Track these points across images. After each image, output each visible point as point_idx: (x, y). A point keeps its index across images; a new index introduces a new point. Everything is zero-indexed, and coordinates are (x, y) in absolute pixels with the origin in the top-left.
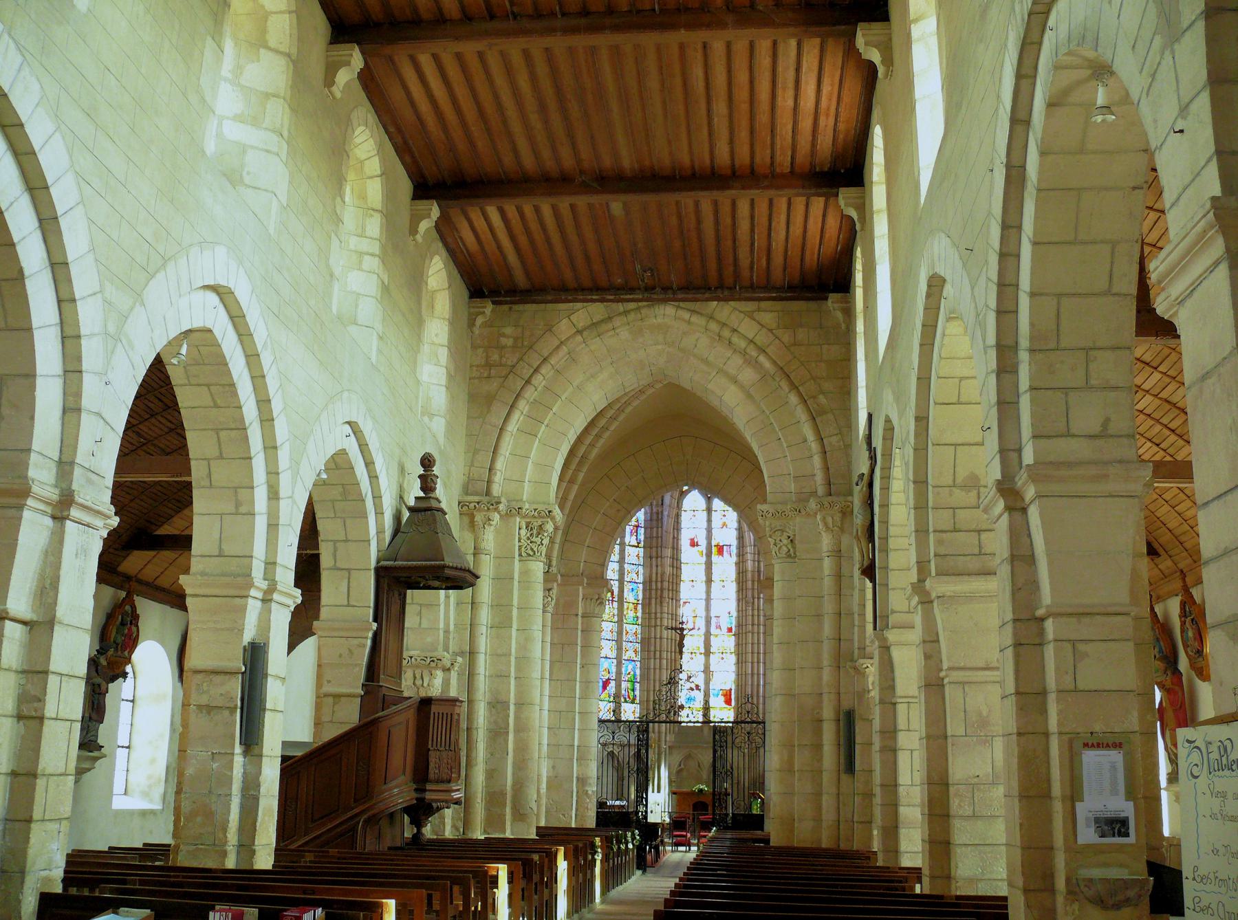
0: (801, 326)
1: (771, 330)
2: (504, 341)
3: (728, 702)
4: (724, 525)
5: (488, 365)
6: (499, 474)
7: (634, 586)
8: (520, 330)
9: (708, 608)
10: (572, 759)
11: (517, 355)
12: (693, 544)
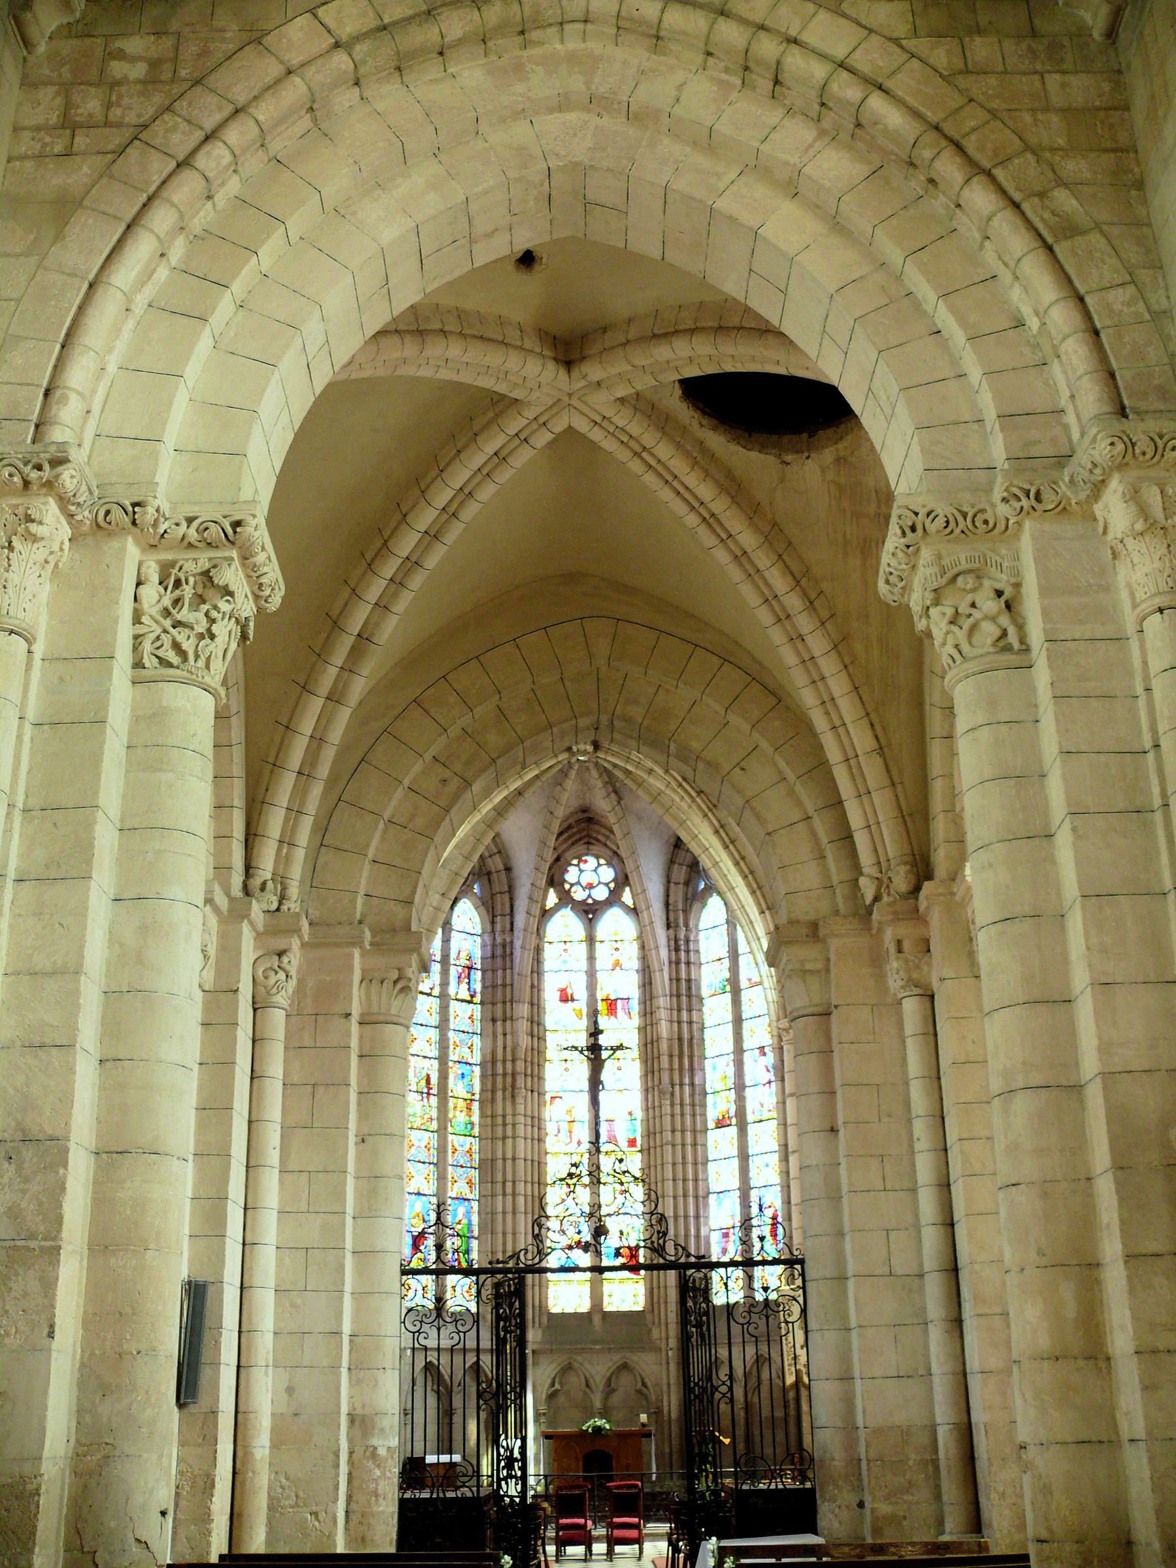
0: (979, 31)
1: (896, 41)
2: (118, 68)
4: (617, 964)
5: (69, 124)
6: (73, 398)
7: (465, 1069)
8: (168, 42)
10: (335, 1367)
11: (158, 99)
12: (565, 998)
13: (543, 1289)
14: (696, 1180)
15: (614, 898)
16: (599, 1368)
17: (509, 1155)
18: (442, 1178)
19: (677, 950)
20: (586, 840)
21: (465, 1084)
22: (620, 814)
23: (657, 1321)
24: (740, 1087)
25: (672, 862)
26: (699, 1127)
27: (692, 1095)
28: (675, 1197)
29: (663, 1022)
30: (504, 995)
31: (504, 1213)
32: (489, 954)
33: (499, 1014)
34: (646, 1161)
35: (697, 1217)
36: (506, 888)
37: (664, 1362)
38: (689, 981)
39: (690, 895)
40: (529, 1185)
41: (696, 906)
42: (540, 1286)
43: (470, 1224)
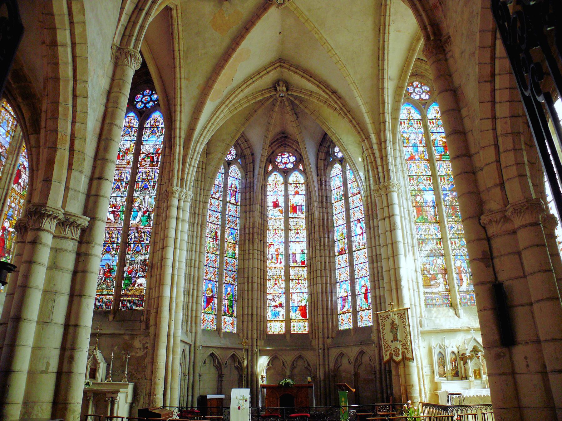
3: (304, 315)
7: (233, 231)
9: (287, 248)
13: (265, 324)
14: (331, 277)
15: (295, 168)
16: (289, 358)
17: (251, 266)
18: (221, 274)
19: (321, 184)
21: (232, 237)
22: (298, 124)
23: (314, 337)
24: (349, 237)
25: (319, 151)
27: (329, 242)
28: (322, 284)
30: (250, 202)
31: (248, 291)
32: (244, 186)
33: (248, 209)
34: (309, 270)
35: (331, 293)
36: (251, 161)
37: (317, 354)
38: (326, 197)
40: (259, 279)
41: (329, 168)
42: (263, 322)
43: (233, 295)
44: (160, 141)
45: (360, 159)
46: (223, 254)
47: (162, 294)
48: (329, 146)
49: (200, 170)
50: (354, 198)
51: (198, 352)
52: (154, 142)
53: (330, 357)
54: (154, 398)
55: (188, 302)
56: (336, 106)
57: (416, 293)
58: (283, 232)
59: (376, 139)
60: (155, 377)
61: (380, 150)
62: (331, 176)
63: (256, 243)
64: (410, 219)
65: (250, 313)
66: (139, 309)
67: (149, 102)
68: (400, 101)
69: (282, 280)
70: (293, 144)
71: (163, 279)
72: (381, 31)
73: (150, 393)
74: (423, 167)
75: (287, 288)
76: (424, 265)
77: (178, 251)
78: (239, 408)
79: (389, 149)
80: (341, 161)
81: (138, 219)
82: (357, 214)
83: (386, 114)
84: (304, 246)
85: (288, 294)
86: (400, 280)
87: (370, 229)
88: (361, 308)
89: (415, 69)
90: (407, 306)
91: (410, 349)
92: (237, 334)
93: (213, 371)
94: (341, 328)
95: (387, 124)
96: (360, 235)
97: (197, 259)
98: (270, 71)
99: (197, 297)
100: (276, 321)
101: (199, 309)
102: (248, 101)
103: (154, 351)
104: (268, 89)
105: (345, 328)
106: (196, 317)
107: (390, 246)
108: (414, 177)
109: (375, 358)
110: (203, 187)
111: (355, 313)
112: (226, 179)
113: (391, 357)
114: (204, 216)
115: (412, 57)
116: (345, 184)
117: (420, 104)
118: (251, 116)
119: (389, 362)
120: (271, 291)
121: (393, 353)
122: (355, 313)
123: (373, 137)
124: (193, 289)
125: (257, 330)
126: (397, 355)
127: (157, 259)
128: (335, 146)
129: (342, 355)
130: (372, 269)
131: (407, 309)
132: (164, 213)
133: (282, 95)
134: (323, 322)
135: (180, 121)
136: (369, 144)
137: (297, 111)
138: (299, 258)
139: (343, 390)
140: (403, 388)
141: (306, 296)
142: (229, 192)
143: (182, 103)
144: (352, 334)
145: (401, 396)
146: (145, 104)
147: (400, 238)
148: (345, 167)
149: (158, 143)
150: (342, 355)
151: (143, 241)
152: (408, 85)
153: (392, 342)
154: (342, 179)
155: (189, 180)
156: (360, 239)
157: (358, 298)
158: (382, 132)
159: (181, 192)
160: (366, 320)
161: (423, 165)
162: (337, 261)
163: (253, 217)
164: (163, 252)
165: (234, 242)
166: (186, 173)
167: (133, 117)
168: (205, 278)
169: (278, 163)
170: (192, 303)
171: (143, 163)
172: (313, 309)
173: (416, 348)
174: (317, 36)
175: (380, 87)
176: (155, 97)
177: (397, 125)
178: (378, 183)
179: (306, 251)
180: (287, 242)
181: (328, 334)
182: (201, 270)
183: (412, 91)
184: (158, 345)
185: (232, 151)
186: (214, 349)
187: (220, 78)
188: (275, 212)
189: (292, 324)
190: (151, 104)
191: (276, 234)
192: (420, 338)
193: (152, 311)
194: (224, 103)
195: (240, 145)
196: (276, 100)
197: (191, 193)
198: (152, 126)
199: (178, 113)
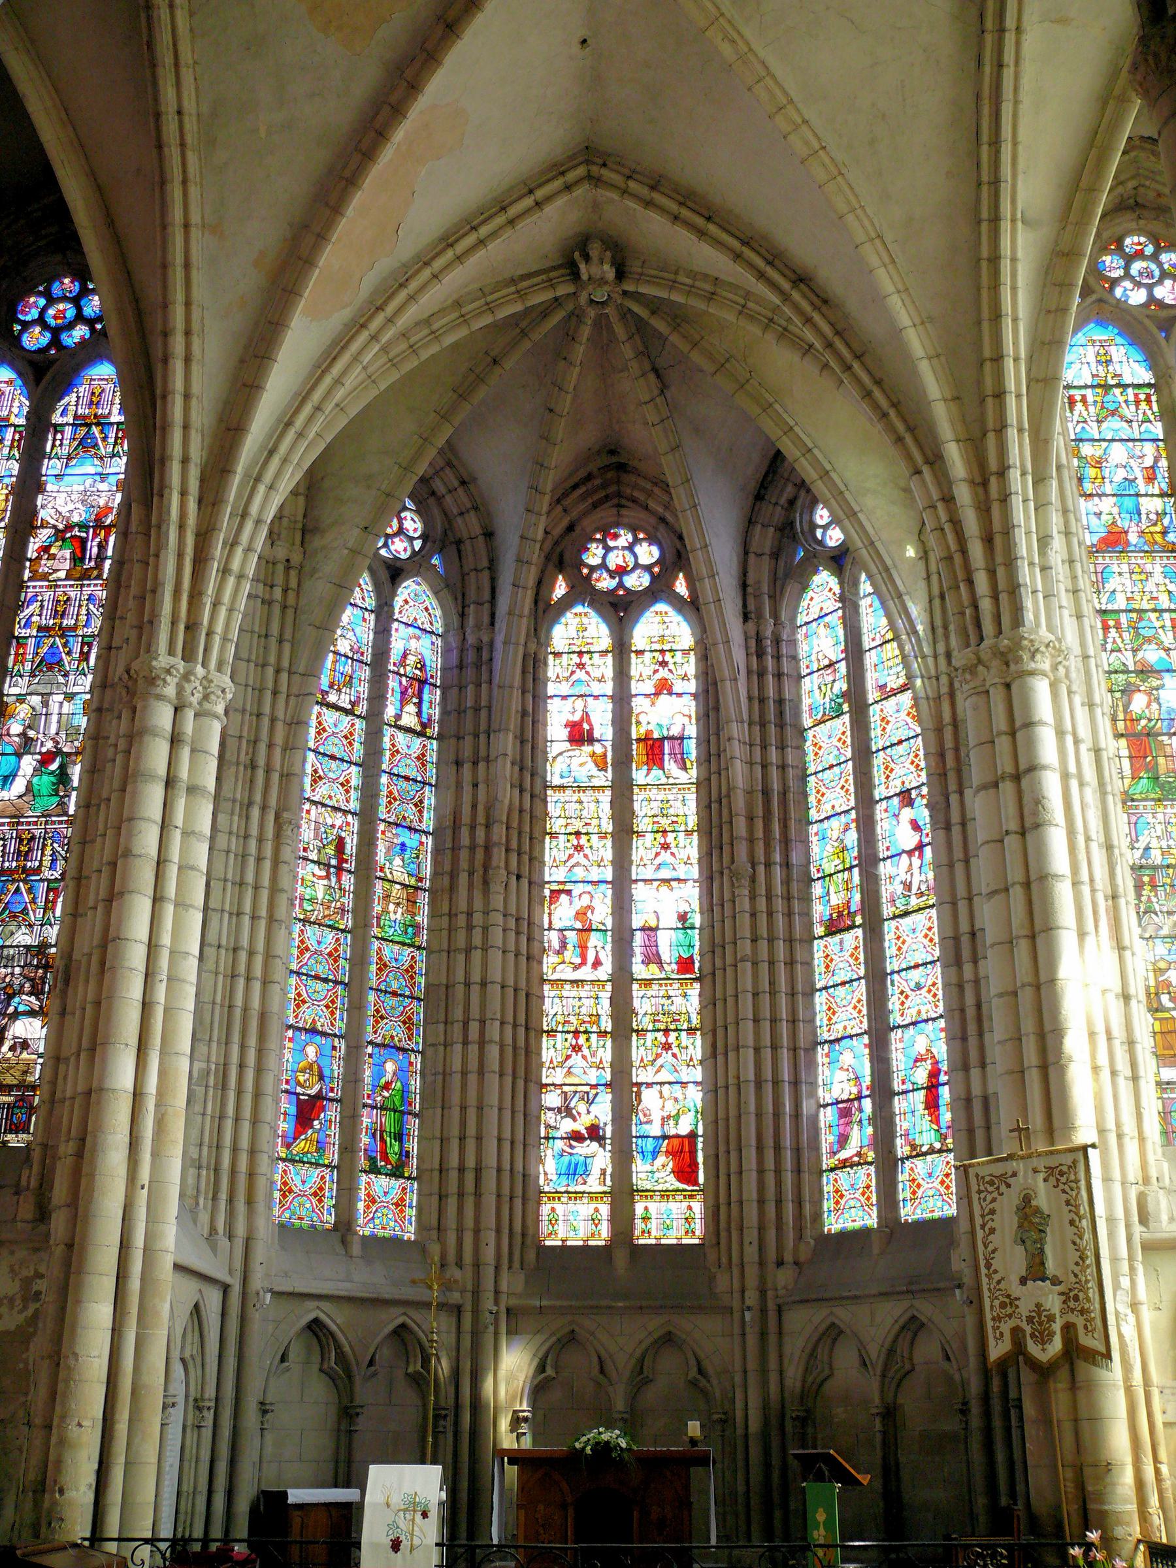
3: (686, 1173)
9: (622, 904)
12: (579, 735)
13: (531, 1205)
14: (793, 1021)
17: (476, 977)
18: (356, 1008)
19: (760, 654)
20: (615, 501)
21: (404, 858)
23: (724, 1260)
24: (868, 860)
25: (750, 522)
26: (798, 933)
27: (787, 882)
28: (757, 1050)
29: (738, 763)
31: (464, 1074)
35: (795, 1083)
36: (485, 563)
38: (780, 702)
39: (780, 573)
41: (791, 587)
42: (524, 1199)
43: (405, 1091)
44: (113, 480)
45: (911, 552)
46: (367, 926)
47: (102, 1078)
48: (792, 502)
49: (278, 593)
50: (890, 705)
51: (256, 1316)
52: (89, 481)
53: (787, 1340)
54: (55, 1503)
55: (222, 1117)
56: (809, 335)
57: (1125, 1087)
58: (609, 842)
59: (968, 463)
60: (63, 1418)
61: (984, 509)
62: (801, 619)
63: (497, 887)
64: (1101, 784)
65: (471, 1162)
66: (15, 1141)
67: (70, 326)
68: (1065, 310)
69: (602, 1034)
70: (650, 494)
71: (109, 1019)
72: (989, 24)
73: (43, 1482)
74: (1158, 577)
75: (621, 1066)
76: (1158, 971)
77: (169, 910)
78: (396, 1545)
79: (1017, 502)
80: (839, 560)
81: (19, 786)
82: (899, 771)
83: (1009, 364)
84: (689, 897)
85: (623, 1087)
86: (1058, 1033)
87: (948, 827)
88: (913, 1147)
89: (1131, 185)
90: (1084, 1134)
91: (1096, 1315)
92: (418, 1247)
93: (319, 1391)
94: (834, 1224)
95: (1011, 401)
96: (910, 853)
97: (260, 946)
98: (549, 199)
99: (258, 1095)
100: (576, 1196)
101: (264, 1146)
102: (464, 320)
103: (63, 1309)
104: (544, 275)
105: (850, 1226)
106: (251, 1175)
107: (1017, 893)
108: (1123, 618)
109: (965, 1349)
110: (285, 663)
111: (887, 1165)
112: (382, 633)
113: (1019, 1347)
114: (289, 777)
115: (1115, 126)
116: (854, 651)
117: (1147, 322)
118: (480, 379)
119: (1004, 1364)
120: (558, 1076)
121: (1028, 1329)
122: (887, 1165)
123: (955, 455)
124: (242, 1066)
125: (498, 1231)
126: (1043, 1338)
127: (86, 942)
128: (814, 502)
129: (833, 1333)
130: (955, 990)
131: (1084, 1148)
132: (119, 758)
133: (600, 295)
134: (761, 1201)
135: (187, 396)
136: (939, 483)
137: (661, 363)
138: (669, 945)
139: (820, 1478)
140: (1069, 1474)
141: (695, 1096)
142: (393, 683)
143: (195, 326)
144: (876, 1251)
145: (1058, 1507)
146: (56, 332)
147: (1059, 859)
148: (856, 583)
149: (103, 486)
150: (833, 1333)
151: (37, 871)
152: (1104, 250)
153: (1023, 1281)
154: (841, 632)
155: (219, 628)
156: (908, 870)
157: (899, 1104)
158: (991, 437)
159: (186, 677)
160: (930, 1192)
161: (1158, 569)
162: (818, 956)
163: (487, 781)
164: (108, 912)
165: (413, 882)
166: (208, 602)
167: (9, 383)
168: (291, 1021)
169: (593, 569)
170: (237, 1119)
171: (45, 566)
172: (722, 1148)
173: (1124, 1309)
174: (726, 49)
175: (985, 253)
176: (93, 305)
177: (1052, 404)
178: (973, 639)
179: (696, 919)
180: (619, 880)
181: (780, 1247)
182: (276, 988)
183: (1121, 272)
184: (79, 1285)
185: (408, 525)
186: (326, 1305)
187: (343, 225)
188: (575, 762)
189: (639, 1208)
190: (80, 332)
191: (578, 848)
192: (1140, 1269)
193: (62, 1149)
194: (363, 326)
195: (439, 499)
196: (576, 316)
197: (226, 681)
198: (81, 422)
199: (178, 366)
